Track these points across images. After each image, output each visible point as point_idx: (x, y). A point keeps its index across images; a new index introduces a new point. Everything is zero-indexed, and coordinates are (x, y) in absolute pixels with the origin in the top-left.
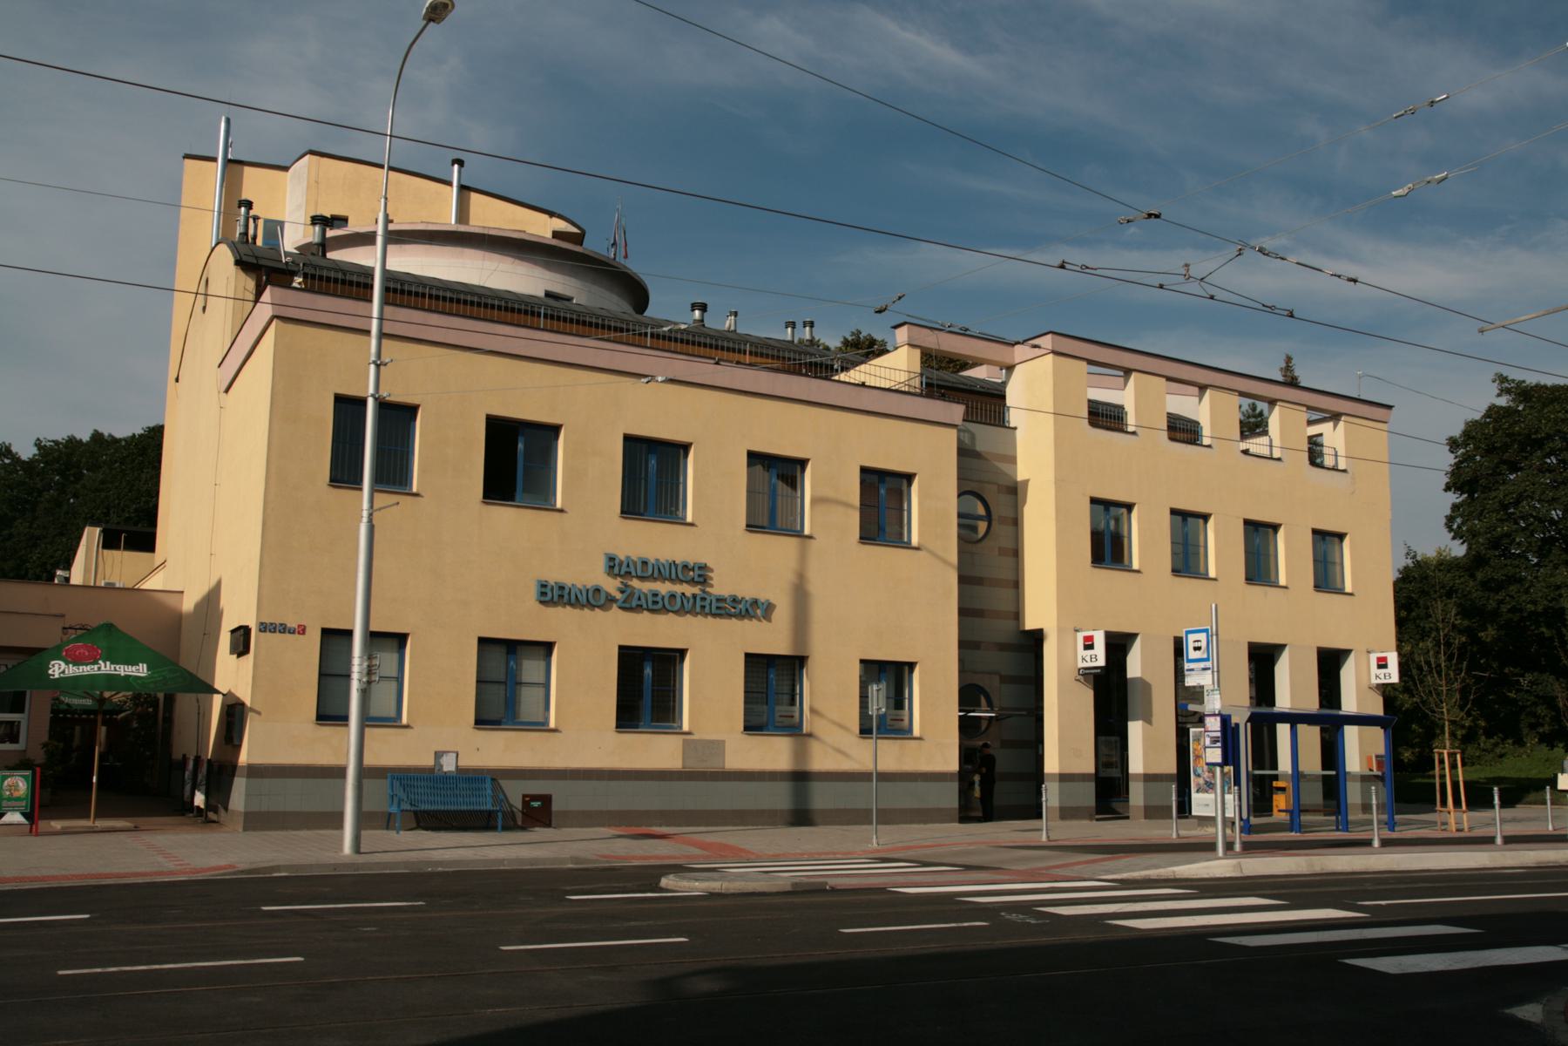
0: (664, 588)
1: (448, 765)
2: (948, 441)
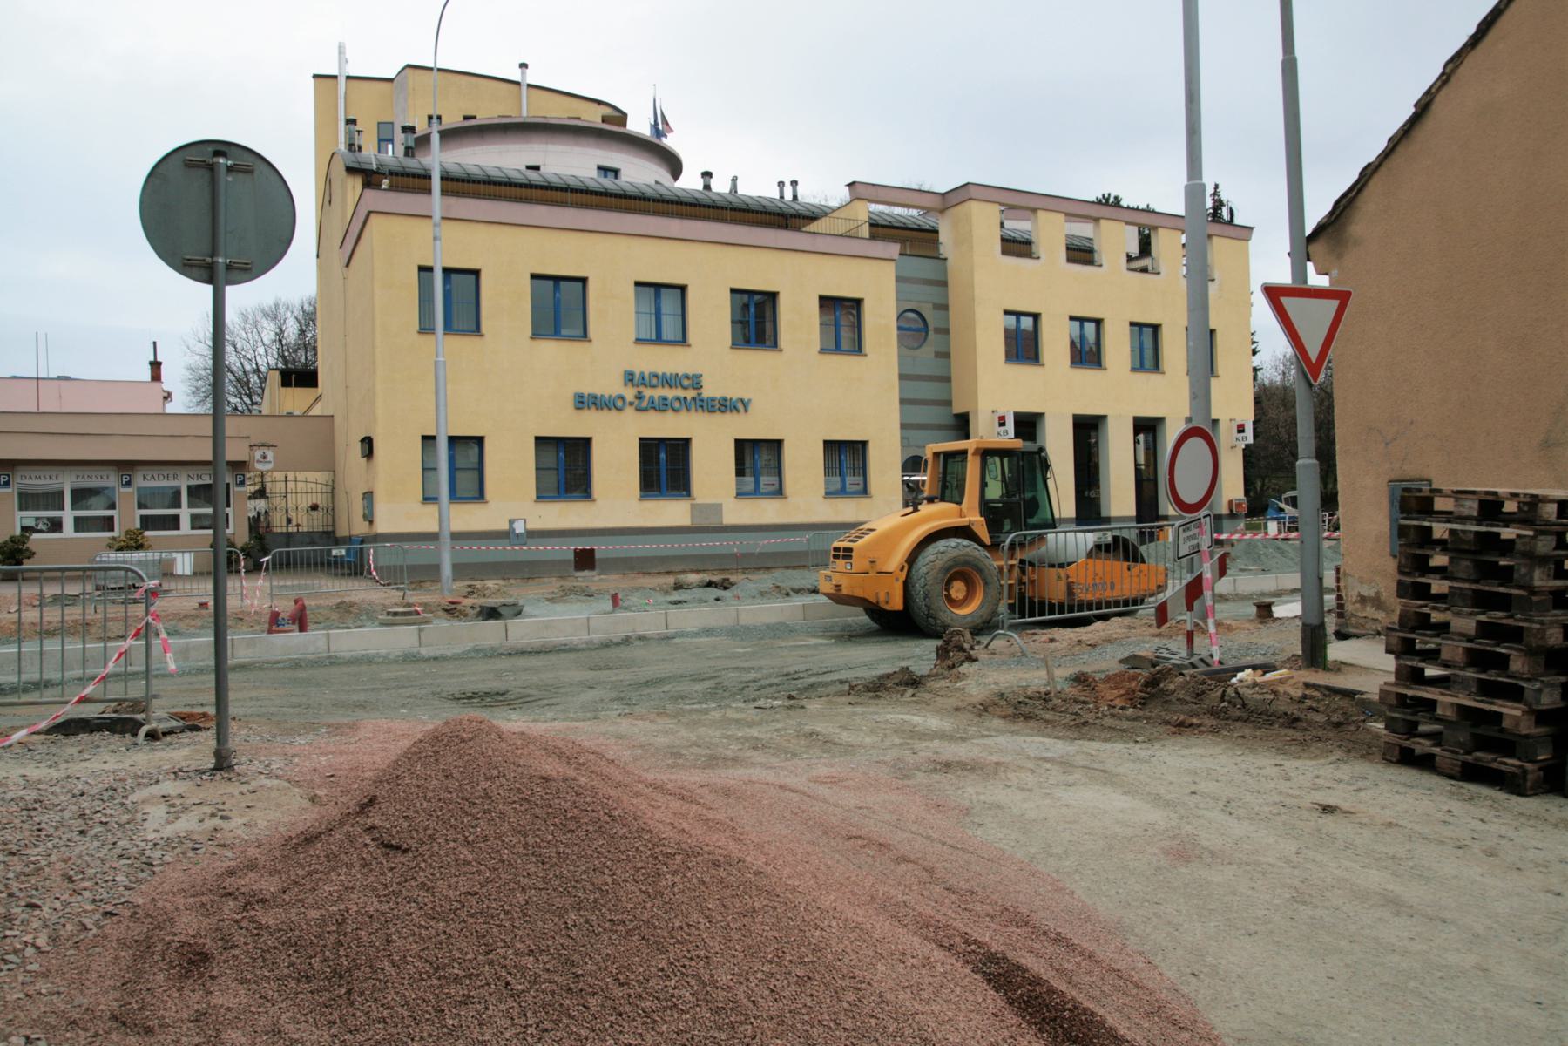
0: (670, 393)
1: (519, 528)
2: (888, 272)
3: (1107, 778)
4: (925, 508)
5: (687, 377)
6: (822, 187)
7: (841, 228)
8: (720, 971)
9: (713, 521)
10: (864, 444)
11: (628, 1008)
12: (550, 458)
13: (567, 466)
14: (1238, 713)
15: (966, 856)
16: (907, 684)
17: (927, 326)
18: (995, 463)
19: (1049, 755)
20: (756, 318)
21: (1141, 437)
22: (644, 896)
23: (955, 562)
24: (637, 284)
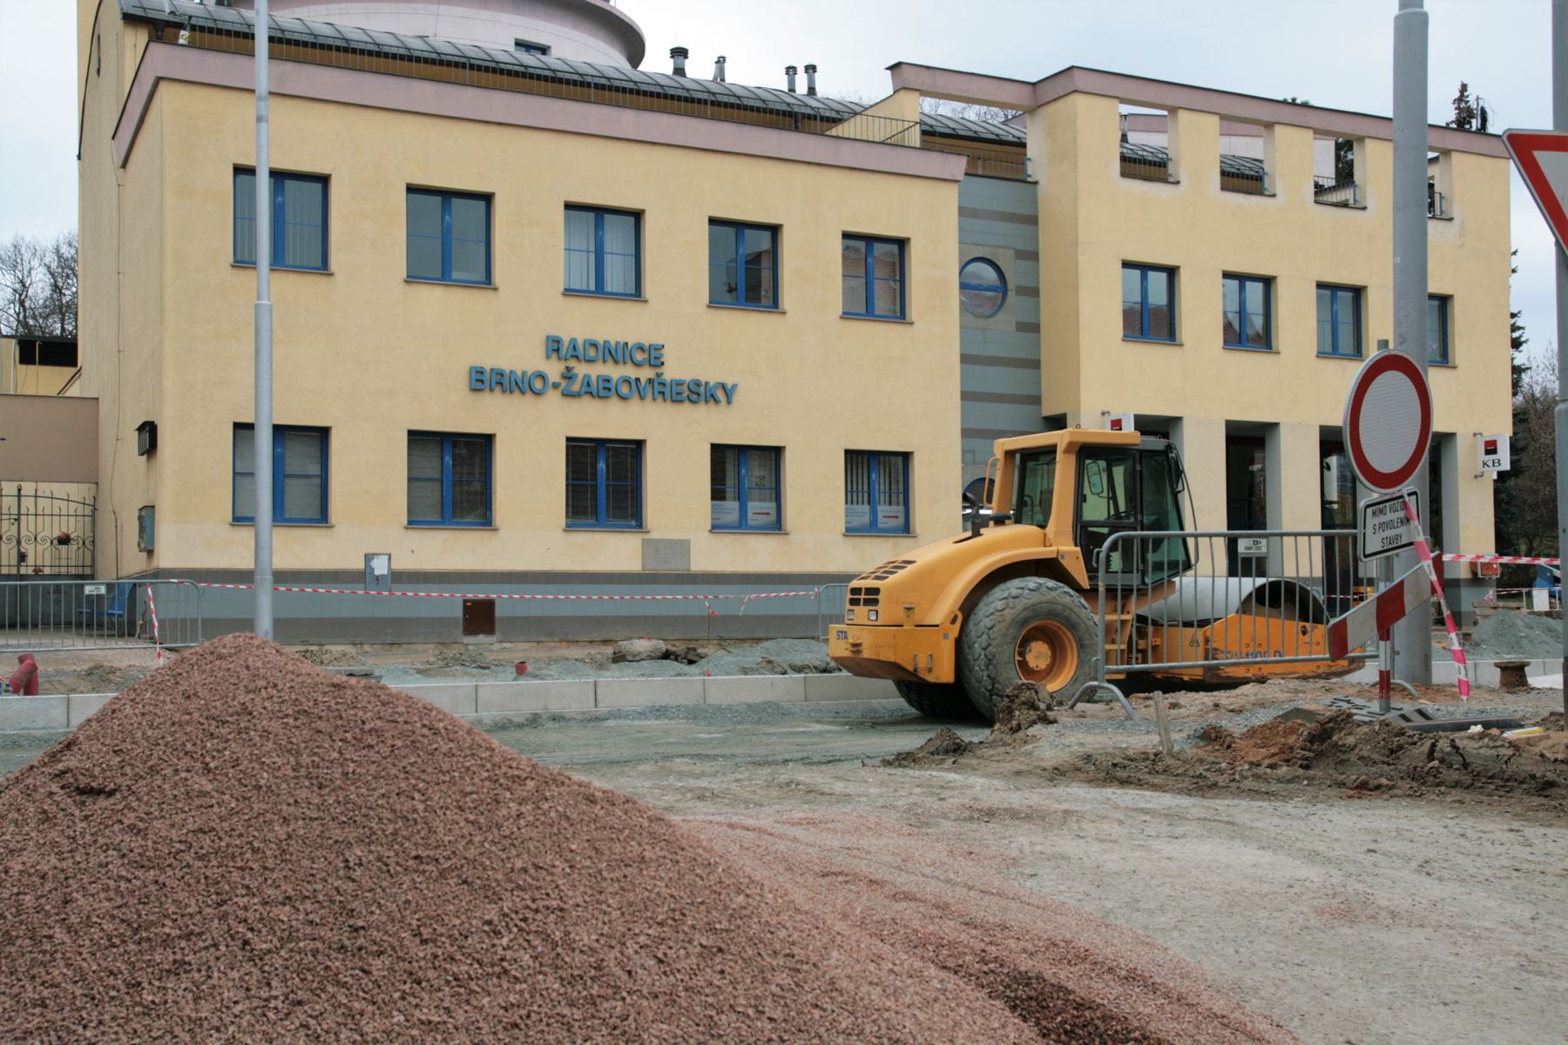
0: (615, 372)
2: (947, 200)
3: (1236, 832)
4: (991, 533)
5: (641, 348)
6: (852, 78)
7: (879, 132)
8: (581, 929)
9: (675, 567)
10: (906, 457)
11: (431, 974)
12: (431, 468)
13: (455, 473)
14: (1455, 776)
15: (1003, 903)
16: (947, 752)
17: (1007, 284)
18: (1096, 468)
19: (1149, 806)
20: (747, 268)
21: (1333, 461)
22: (471, 828)
23: (1034, 612)
24: (569, 206)
